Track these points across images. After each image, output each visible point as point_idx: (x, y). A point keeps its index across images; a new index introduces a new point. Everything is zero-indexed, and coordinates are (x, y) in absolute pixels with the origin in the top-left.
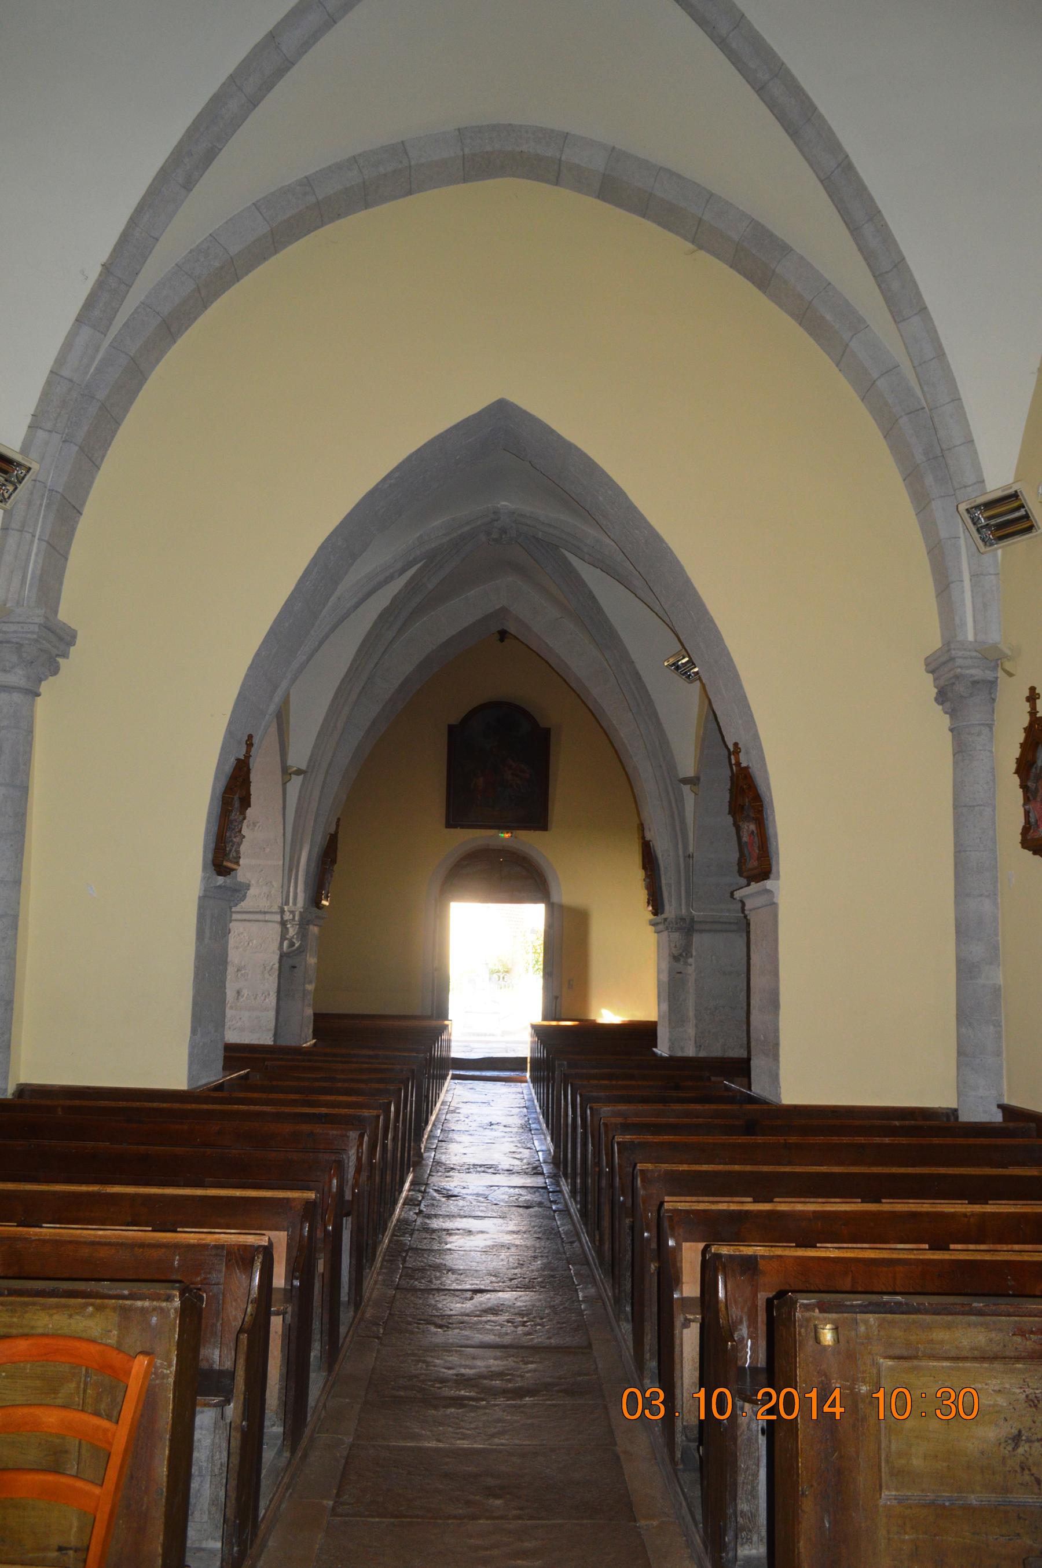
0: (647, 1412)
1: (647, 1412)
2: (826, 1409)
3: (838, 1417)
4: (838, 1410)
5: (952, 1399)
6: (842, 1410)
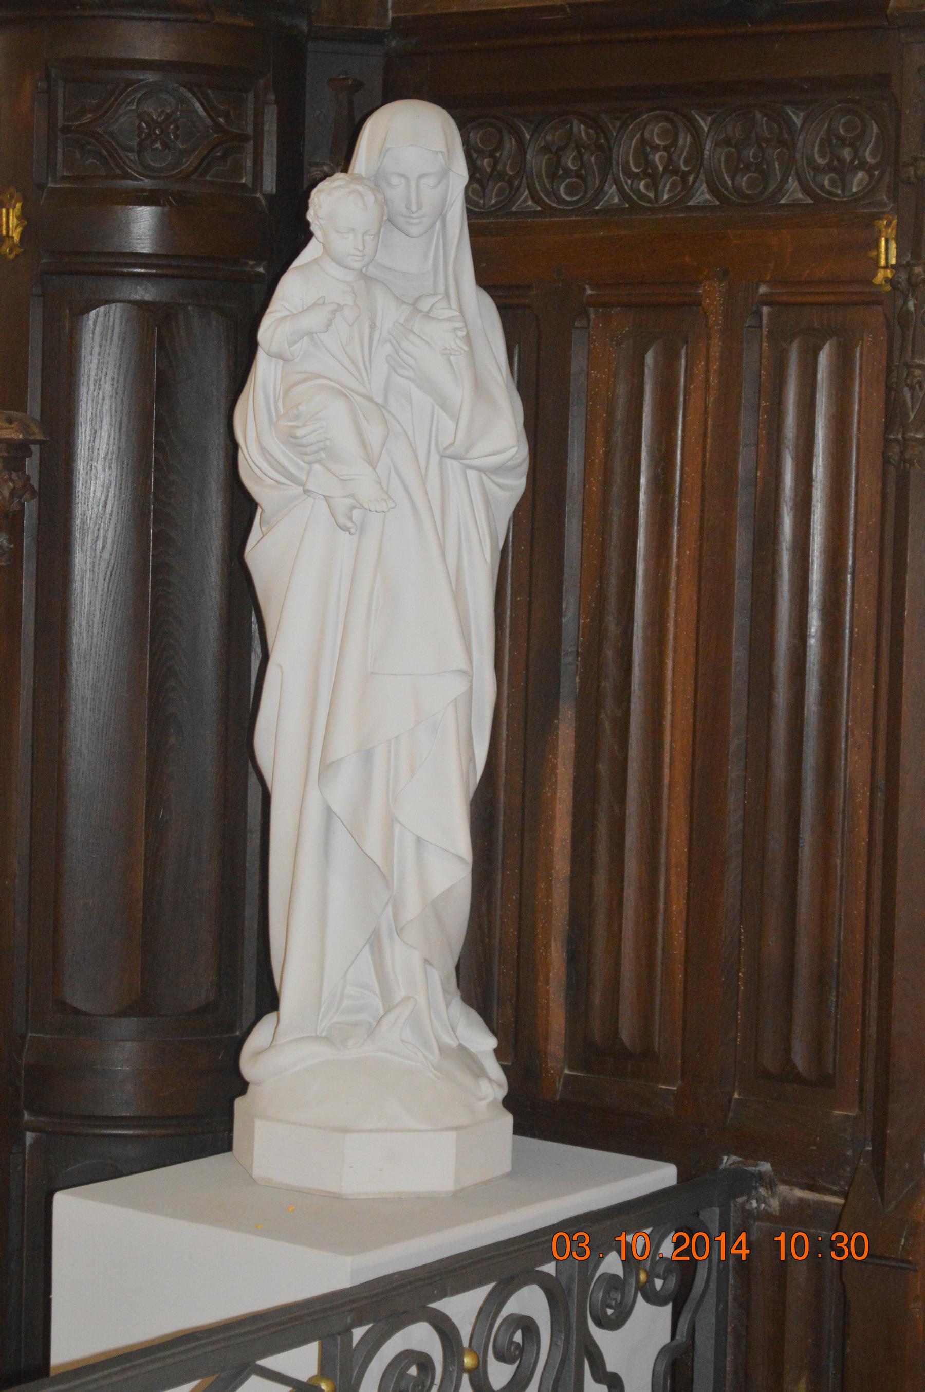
0: (574, 1253)
1: (574, 1253)
2: (733, 1251)
3: (744, 1258)
4: (744, 1252)
5: (587, 1242)
6: (748, 1252)
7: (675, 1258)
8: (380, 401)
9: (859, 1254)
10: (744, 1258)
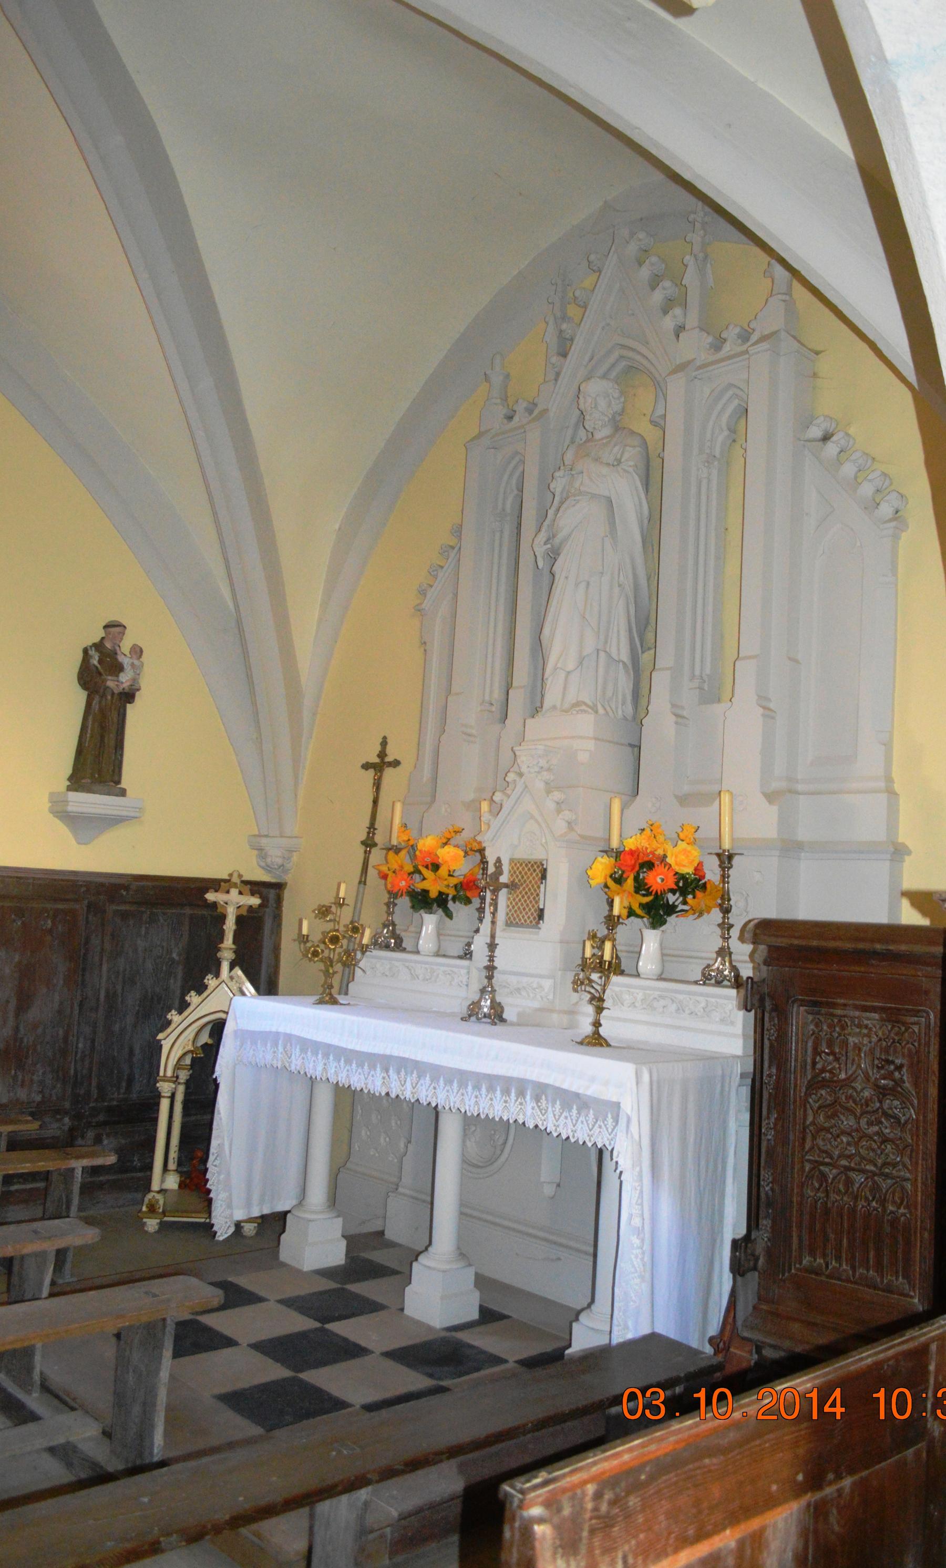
2: (827, 1409)
3: (838, 1417)
6: (843, 1410)
7: (760, 1417)
8: (774, 293)
9: (902, 1412)
10: (838, 1417)
